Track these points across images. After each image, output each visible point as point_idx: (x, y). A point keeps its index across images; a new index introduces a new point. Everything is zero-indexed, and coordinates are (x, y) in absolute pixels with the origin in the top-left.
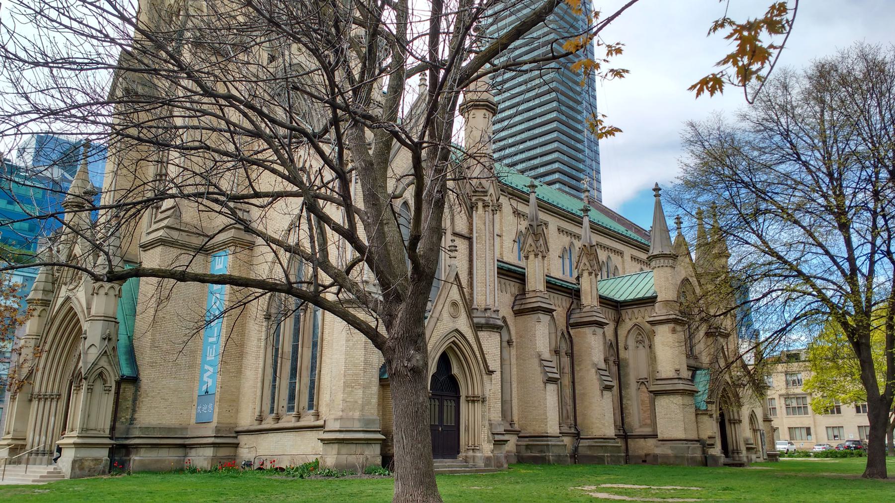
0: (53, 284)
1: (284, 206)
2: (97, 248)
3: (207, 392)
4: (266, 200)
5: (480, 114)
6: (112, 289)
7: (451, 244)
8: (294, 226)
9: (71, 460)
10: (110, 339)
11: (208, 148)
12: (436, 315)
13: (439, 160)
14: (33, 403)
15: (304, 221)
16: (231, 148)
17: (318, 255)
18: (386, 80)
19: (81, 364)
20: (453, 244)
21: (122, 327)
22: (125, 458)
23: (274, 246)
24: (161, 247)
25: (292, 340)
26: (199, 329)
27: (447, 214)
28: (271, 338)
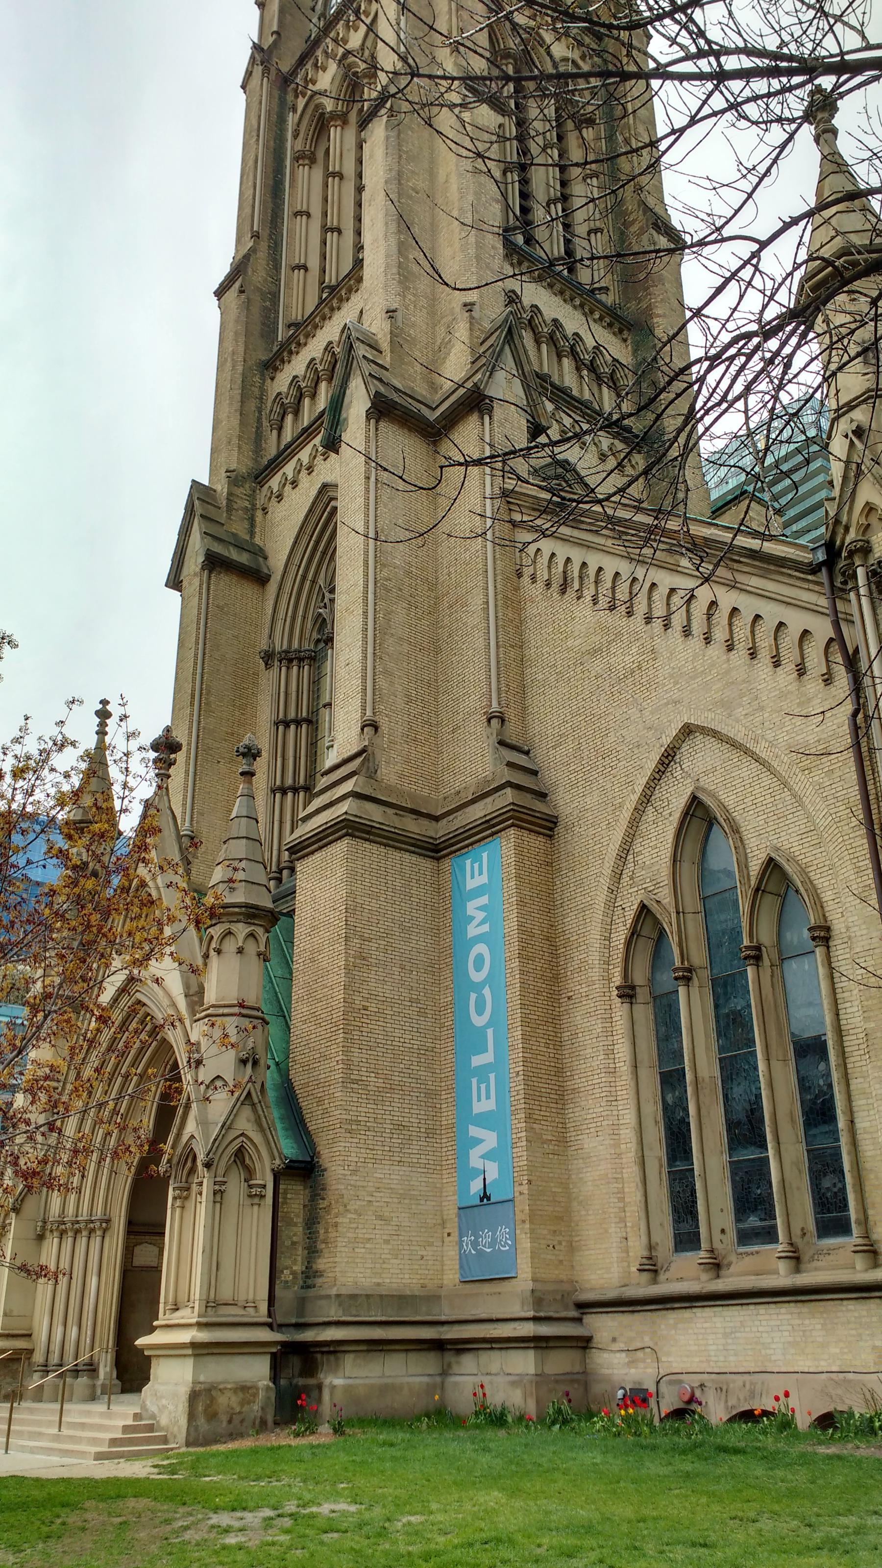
6: (251, 941)
9: (184, 1391)
14: (46, 1243)
22: (301, 1381)
24: (346, 841)
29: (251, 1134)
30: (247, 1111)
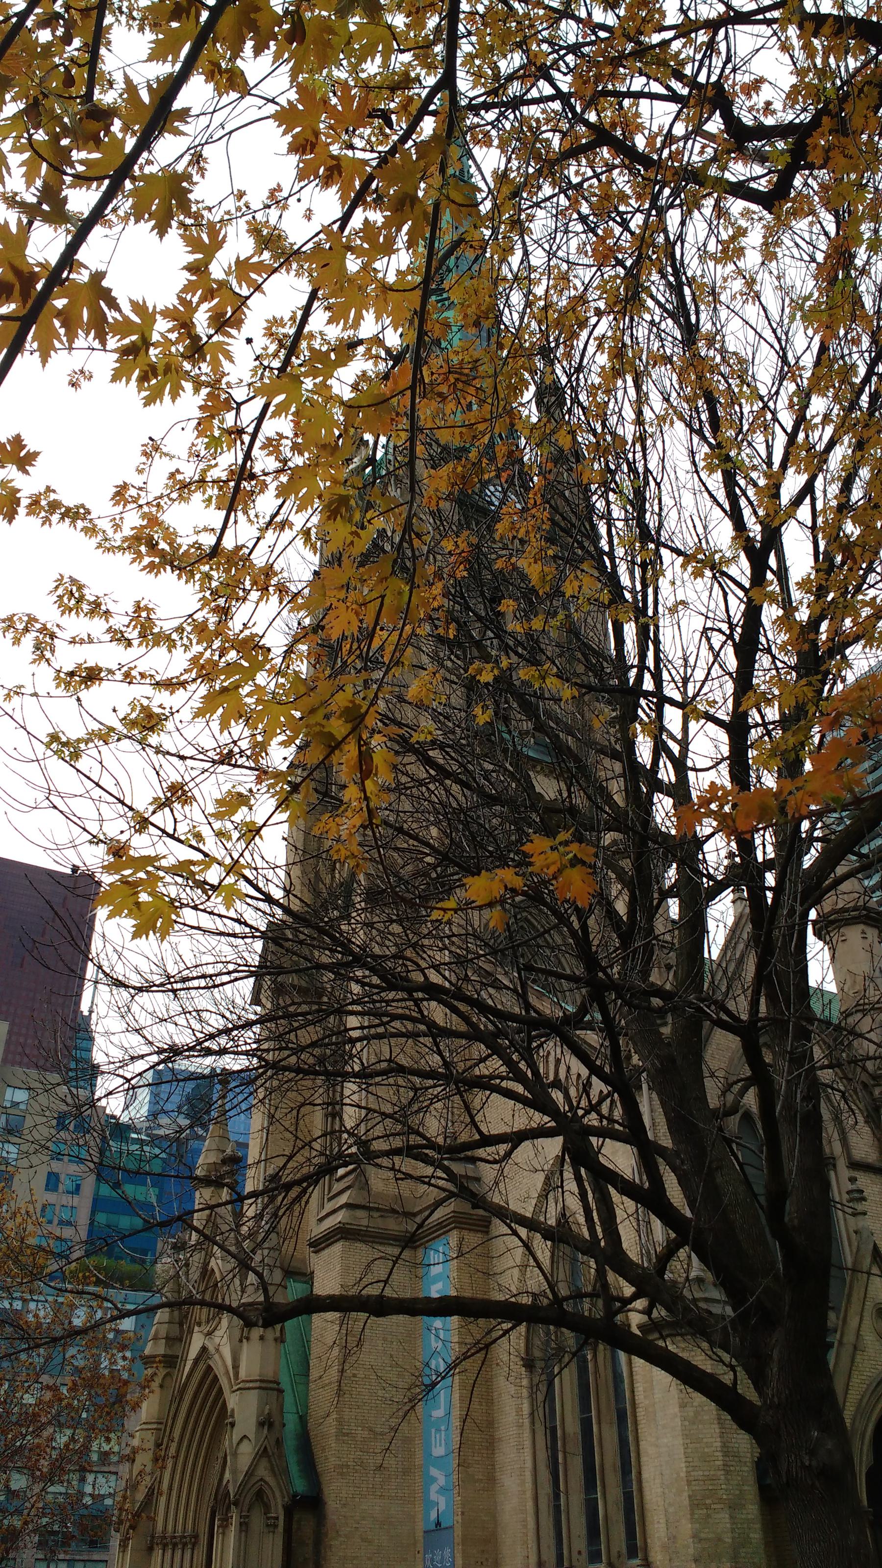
0: (181, 1324)
1: (532, 1154)
2: (244, 1265)
3: (438, 1524)
4: (503, 1148)
5: (854, 933)
7: (850, 1187)
8: (552, 1185)
10: (271, 1425)
11: (401, 1070)
12: (850, 1338)
13: (795, 1038)
14: (154, 1554)
15: (568, 1174)
16: (435, 1060)
17: (603, 1244)
18: (674, 907)
19: (227, 1475)
20: (854, 1187)
21: (288, 1398)
23: (523, 1232)
25: (578, 1409)
26: (413, 1402)
27: (830, 1130)
28: (541, 1410)
29: (267, 1479)
30: (264, 1463)
